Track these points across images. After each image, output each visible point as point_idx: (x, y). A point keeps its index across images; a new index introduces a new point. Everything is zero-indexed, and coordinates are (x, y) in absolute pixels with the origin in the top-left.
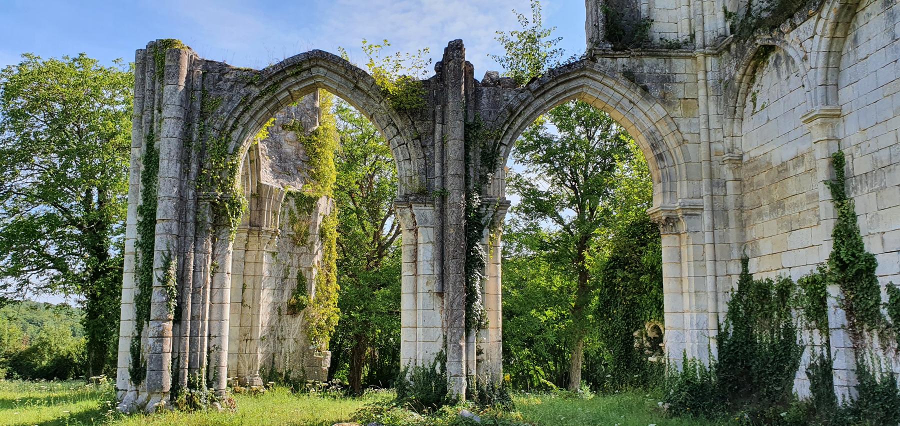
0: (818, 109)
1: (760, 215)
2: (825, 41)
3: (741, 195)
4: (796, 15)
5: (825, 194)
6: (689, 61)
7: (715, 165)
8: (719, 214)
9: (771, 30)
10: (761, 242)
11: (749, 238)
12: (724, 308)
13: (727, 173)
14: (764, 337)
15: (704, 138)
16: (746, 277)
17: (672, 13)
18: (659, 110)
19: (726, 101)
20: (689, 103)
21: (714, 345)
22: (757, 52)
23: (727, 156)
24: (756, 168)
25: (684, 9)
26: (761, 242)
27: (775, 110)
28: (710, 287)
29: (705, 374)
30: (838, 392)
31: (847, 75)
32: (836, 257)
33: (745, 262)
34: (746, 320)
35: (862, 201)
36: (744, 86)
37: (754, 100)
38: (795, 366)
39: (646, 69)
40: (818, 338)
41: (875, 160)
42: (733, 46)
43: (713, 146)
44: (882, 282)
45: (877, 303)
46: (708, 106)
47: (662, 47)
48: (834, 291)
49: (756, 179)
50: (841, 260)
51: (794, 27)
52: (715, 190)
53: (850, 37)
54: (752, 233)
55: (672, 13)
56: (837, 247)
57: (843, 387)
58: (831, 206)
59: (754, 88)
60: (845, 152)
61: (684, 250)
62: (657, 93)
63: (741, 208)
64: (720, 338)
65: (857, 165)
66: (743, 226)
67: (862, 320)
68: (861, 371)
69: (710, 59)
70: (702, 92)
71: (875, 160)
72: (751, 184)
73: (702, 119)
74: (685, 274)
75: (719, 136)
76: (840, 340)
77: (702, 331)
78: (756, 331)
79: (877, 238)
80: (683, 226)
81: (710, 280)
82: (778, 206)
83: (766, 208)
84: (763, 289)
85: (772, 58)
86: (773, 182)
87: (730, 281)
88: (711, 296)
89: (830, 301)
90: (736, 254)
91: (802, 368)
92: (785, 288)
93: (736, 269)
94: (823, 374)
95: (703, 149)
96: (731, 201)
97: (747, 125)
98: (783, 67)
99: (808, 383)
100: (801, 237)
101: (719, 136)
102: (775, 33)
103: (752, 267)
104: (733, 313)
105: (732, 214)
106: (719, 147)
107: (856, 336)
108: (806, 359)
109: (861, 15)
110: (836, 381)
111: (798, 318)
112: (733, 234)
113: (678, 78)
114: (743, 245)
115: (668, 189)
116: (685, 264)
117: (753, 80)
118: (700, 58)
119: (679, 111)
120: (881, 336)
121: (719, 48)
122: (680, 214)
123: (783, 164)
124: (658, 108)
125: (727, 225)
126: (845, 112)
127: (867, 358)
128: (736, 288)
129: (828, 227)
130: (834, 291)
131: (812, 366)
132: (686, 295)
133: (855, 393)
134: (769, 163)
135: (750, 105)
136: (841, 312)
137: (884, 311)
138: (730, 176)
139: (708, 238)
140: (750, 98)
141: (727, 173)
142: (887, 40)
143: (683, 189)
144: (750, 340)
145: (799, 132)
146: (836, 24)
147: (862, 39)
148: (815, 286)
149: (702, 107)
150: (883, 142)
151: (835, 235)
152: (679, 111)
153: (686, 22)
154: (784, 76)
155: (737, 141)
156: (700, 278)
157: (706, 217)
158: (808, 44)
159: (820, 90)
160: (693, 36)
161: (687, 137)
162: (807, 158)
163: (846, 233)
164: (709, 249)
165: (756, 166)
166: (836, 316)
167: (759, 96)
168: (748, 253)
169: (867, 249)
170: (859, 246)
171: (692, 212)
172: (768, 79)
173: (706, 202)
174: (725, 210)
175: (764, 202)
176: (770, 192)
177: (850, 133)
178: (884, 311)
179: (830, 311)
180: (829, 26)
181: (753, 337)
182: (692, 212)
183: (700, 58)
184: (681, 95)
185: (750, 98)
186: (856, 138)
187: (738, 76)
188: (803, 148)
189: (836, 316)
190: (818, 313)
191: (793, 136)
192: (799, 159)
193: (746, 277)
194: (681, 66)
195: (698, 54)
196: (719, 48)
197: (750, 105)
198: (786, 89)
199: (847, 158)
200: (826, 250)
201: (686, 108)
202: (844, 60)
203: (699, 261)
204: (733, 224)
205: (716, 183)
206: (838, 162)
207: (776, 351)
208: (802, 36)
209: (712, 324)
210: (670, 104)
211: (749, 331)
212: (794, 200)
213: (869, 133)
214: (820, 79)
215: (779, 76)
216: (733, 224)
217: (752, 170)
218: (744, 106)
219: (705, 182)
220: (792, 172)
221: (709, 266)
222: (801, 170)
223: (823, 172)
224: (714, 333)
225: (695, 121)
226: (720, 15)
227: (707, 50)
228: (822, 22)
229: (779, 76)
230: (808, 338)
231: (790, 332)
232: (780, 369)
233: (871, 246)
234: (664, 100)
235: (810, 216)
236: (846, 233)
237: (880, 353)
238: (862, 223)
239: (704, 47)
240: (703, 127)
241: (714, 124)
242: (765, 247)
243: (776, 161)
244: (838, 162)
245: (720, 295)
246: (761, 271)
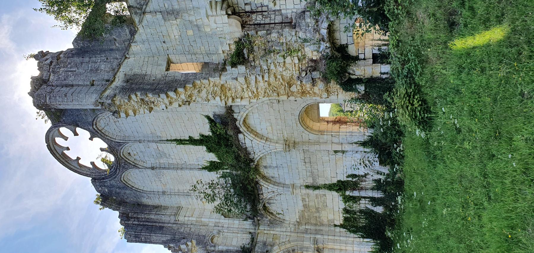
0: (291, 190)
1: (319, 217)
2: (270, 185)
3: (311, 224)
4: (259, 192)
5: (317, 192)
6: (259, 235)
7: (299, 231)
8: (317, 232)
9: (259, 202)
10: (329, 218)
11: (327, 223)
12: (352, 235)
13: (303, 227)
14: (363, 222)
15: (289, 234)
16: (341, 226)
17: (239, 240)
18: (276, 248)
19: (276, 224)
20: (274, 237)
21: (366, 240)
22: (264, 209)
23: (297, 226)
24: (303, 216)
25: (239, 235)
26: (329, 218)
27: (285, 206)
28: (345, 239)
29: (377, 244)
30: (379, 196)
31: (282, 181)
32: (337, 191)
33: (335, 226)
34: (356, 227)
35: (321, 182)
36: (273, 217)
37: (279, 214)
38: (373, 211)
39: (260, 250)
40: (363, 201)
41: (309, 176)
42: (259, 218)
43: (292, 231)
44: (346, 179)
45: (352, 181)
46: (277, 231)
47: (252, 244)
48: (348, 193)
49: (307, 217)
50: (338, 189)
51: (262, 194)
52: (309, 232)
53: (271, 178)
54: (325, 221)
55: (239, 240)
56: (334, 190)
57: (378, 195)
58: (321, 190)
59: (275, 213)
60: (305, 184)
61: (329, 247)
62: (269, 248)
63: (316, 225)
64: (363, 237)
65: (310, 181)
66: (322, 225)
67: (357, 186)
68: (373, 189)
69: (260, 228)
70: (272, 232)
71: (309, 176)
72: (308, 219)
73: (282, 233)
74: (339, 247)
75: (289, 228)
76: (363, 194)
77: (360, 243)
78: (361, 225)
79: (332, 179)
80: (321, 246)
81: (341, 238)
82: (318, 210)
83: (317, 214)
84: (346, 219)
85: (267, 205)
86: (309, 211)
87: (342, 232)
88: (347, 239)
89: (351, 194)
90: (333, 228)
91: (373, 208)
92: (346, 211)
93: (338, 229)
94: (373, 200)
95: (293, 234)
96: (313, 228)
97: (287, 218)
98: (272, 201)
99: (378, 207)
100: (329, 204)
101: (289, 228)
102: (261, 201)
103: (338, 223)
104: (354, 232)
105: (318, 228)
106: (293, 229)
107: (362, 189)
108: (370, 207)
109: (266, 175)
110: (376, 196)
111: (356, 207)
112: (325, 229)
113: (265, 240)
114: (329, 225)
115: (306, 249)
116: (335, 247)
117: (272, 213)
118: (259, 231)
119: (277, 241)
120: (362, 181)
121: (257, 224)
122: (316, 246)
123: (304, 206)
124: (275, 248)
125: (322, 230)
126: (292, 183)
127: (369, 187)
128: (345, 230)
129: (327, 192)
130: (348, 193)
131: (372, 205)
132: (347, 248)
133: (379, 191)
134: (302, 211)
135: (280, 216)
136: (354, 192)
137: (354, 180)
138: (304, 227)
139: (326, 237)
140: (277, 216)
141: (303, 227)
142: (276, 169)
143: (307, 244)
144: (364, 227)
145: (295, 199)
146: (266, 181)
147: (273, 175)
148: (347, 199)
149: (277, 233)
150: (305, 174)
151: (330, 190)
152: (277, 241)
153: (244, 235)
154: (275, 201)
155: (291, 222)
156: (341, 242)
157: (318, 237)
158: (269, 190)
159: (285, 189)
160: (250, 233)
161: (287, 239)
162: (304, 197)
163: (330, 187)
164: (330, 237)
165: (302, 216)
166: (356, 193)
167: (278, 212)
168: (332, 224)
169: (335, 182)
170: (334, 184)
171: (316, 242)
172: (273, 208)
173: (312, 236)
174: (316, 230)
175: (315, 215)
176: (312, 212)
177: (299, 182)
178: (354, 180)
179: (354, 195)
180: (267, 183)
181: (363, 226)
182: (316, 242)
183: (259, 231)
184: (271, 240)
185: (277, 216)
186: (302, 181)
187: (269, 218)
188: (300, 198)
189: (356, 193)
190: (355, 199)
191: (295, 201)
192: (303, 200)
193: (341, 226)
194: (260, 238)
195: (257, 232)
196: (257, 224)
197: (280, 216)
198: (279, 201)
199: (307, 184)
200: (335, 193)
201: (276, 239)
202: (277, 181)
203: (334, 241)
204: (321, 228)
205: (306, 232)
206: (307, 187)
207: (368, 218)
208: (266, 192)
209: (358, 240)
210: (274, 244)
211: (360, 227)
212: (316, 203)
213: (301, 177)
214: (281, 188)
215: (274, 203)
216: (321, 228)
217: (303, 219)
218: (280, 218)
219: (305, 236)
220: (307, 203)
221: (336, 238)
222: (307, 200)
223: (310, 191)
224: (362, 239)
225: (282, 236)
226: (245, 222)
227: (257, 228)
228: (265, 185)
229: (274, 203)
230: (364, 204)
231: (361, 211)
232: (374, 216)
233: (335, 181)
234: (272, 246)
235: (323, 199)
236: (330, 187)
237: (367, 183)
238: (327, 183)
239: (255, 229)
240: (285, 233)
241: (284, 230)
242: (331, 217)
243: (302, 208)
244: (307, 187)
245: (347, 235)
246: (340, 220)
